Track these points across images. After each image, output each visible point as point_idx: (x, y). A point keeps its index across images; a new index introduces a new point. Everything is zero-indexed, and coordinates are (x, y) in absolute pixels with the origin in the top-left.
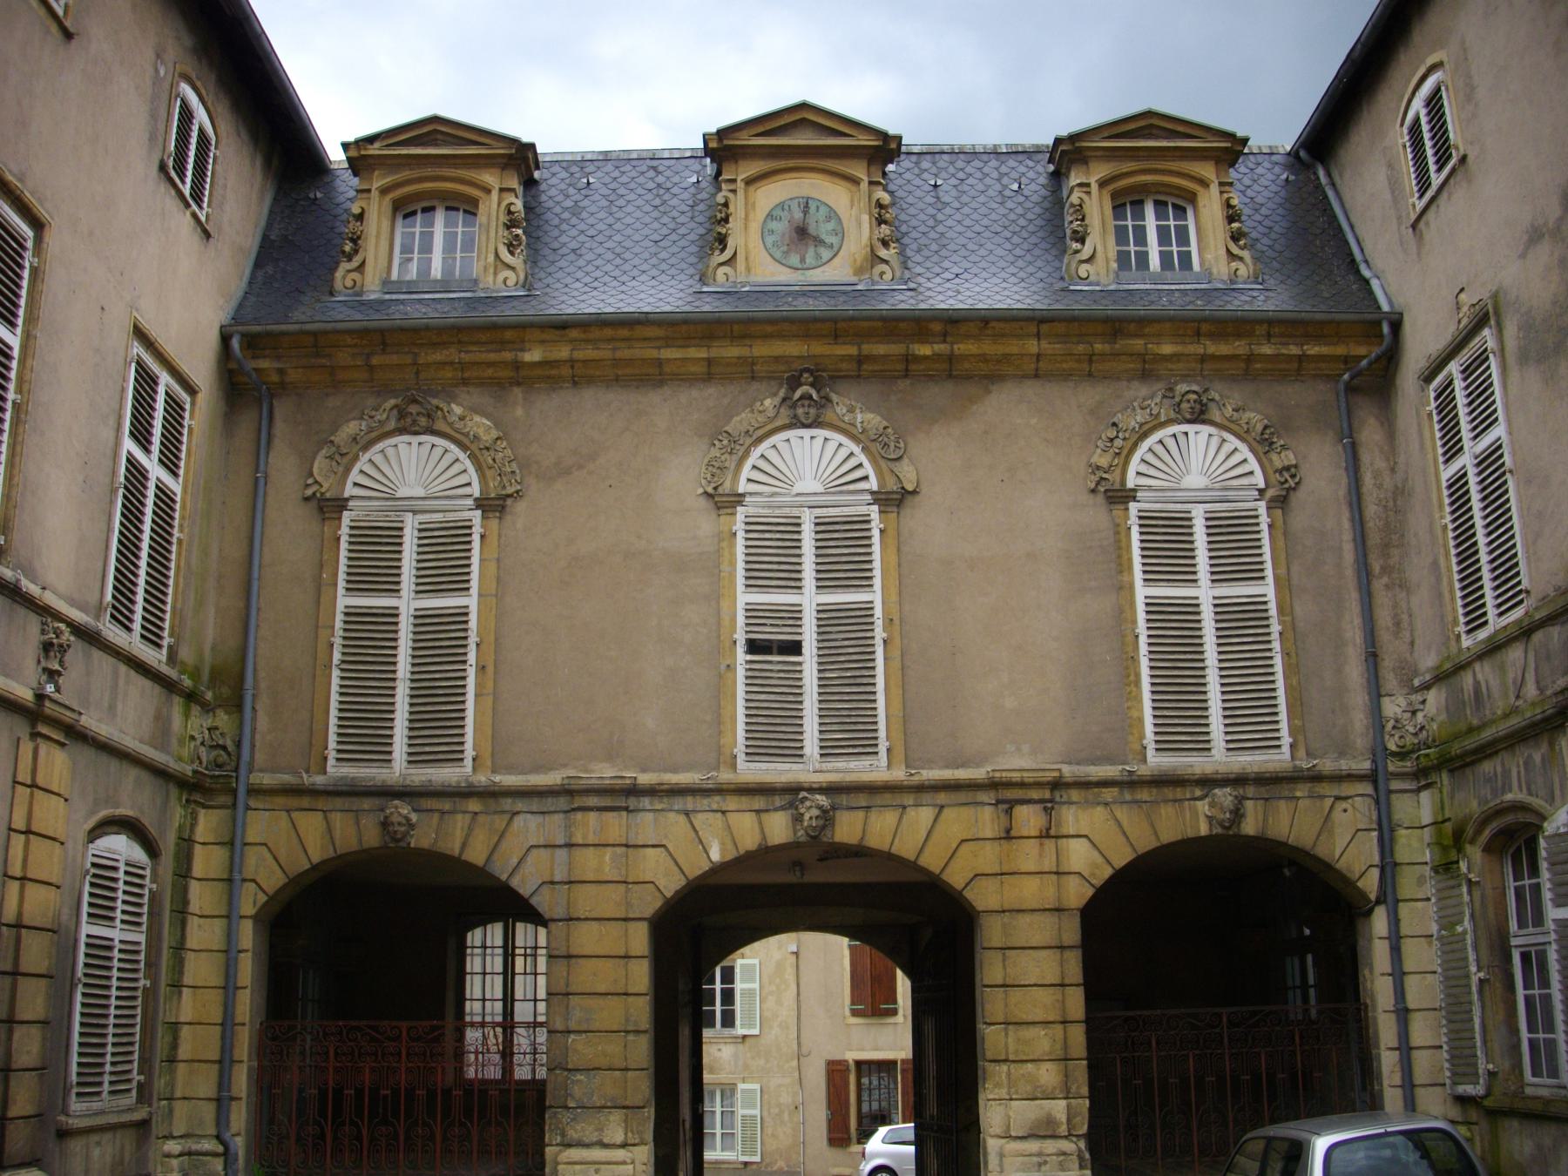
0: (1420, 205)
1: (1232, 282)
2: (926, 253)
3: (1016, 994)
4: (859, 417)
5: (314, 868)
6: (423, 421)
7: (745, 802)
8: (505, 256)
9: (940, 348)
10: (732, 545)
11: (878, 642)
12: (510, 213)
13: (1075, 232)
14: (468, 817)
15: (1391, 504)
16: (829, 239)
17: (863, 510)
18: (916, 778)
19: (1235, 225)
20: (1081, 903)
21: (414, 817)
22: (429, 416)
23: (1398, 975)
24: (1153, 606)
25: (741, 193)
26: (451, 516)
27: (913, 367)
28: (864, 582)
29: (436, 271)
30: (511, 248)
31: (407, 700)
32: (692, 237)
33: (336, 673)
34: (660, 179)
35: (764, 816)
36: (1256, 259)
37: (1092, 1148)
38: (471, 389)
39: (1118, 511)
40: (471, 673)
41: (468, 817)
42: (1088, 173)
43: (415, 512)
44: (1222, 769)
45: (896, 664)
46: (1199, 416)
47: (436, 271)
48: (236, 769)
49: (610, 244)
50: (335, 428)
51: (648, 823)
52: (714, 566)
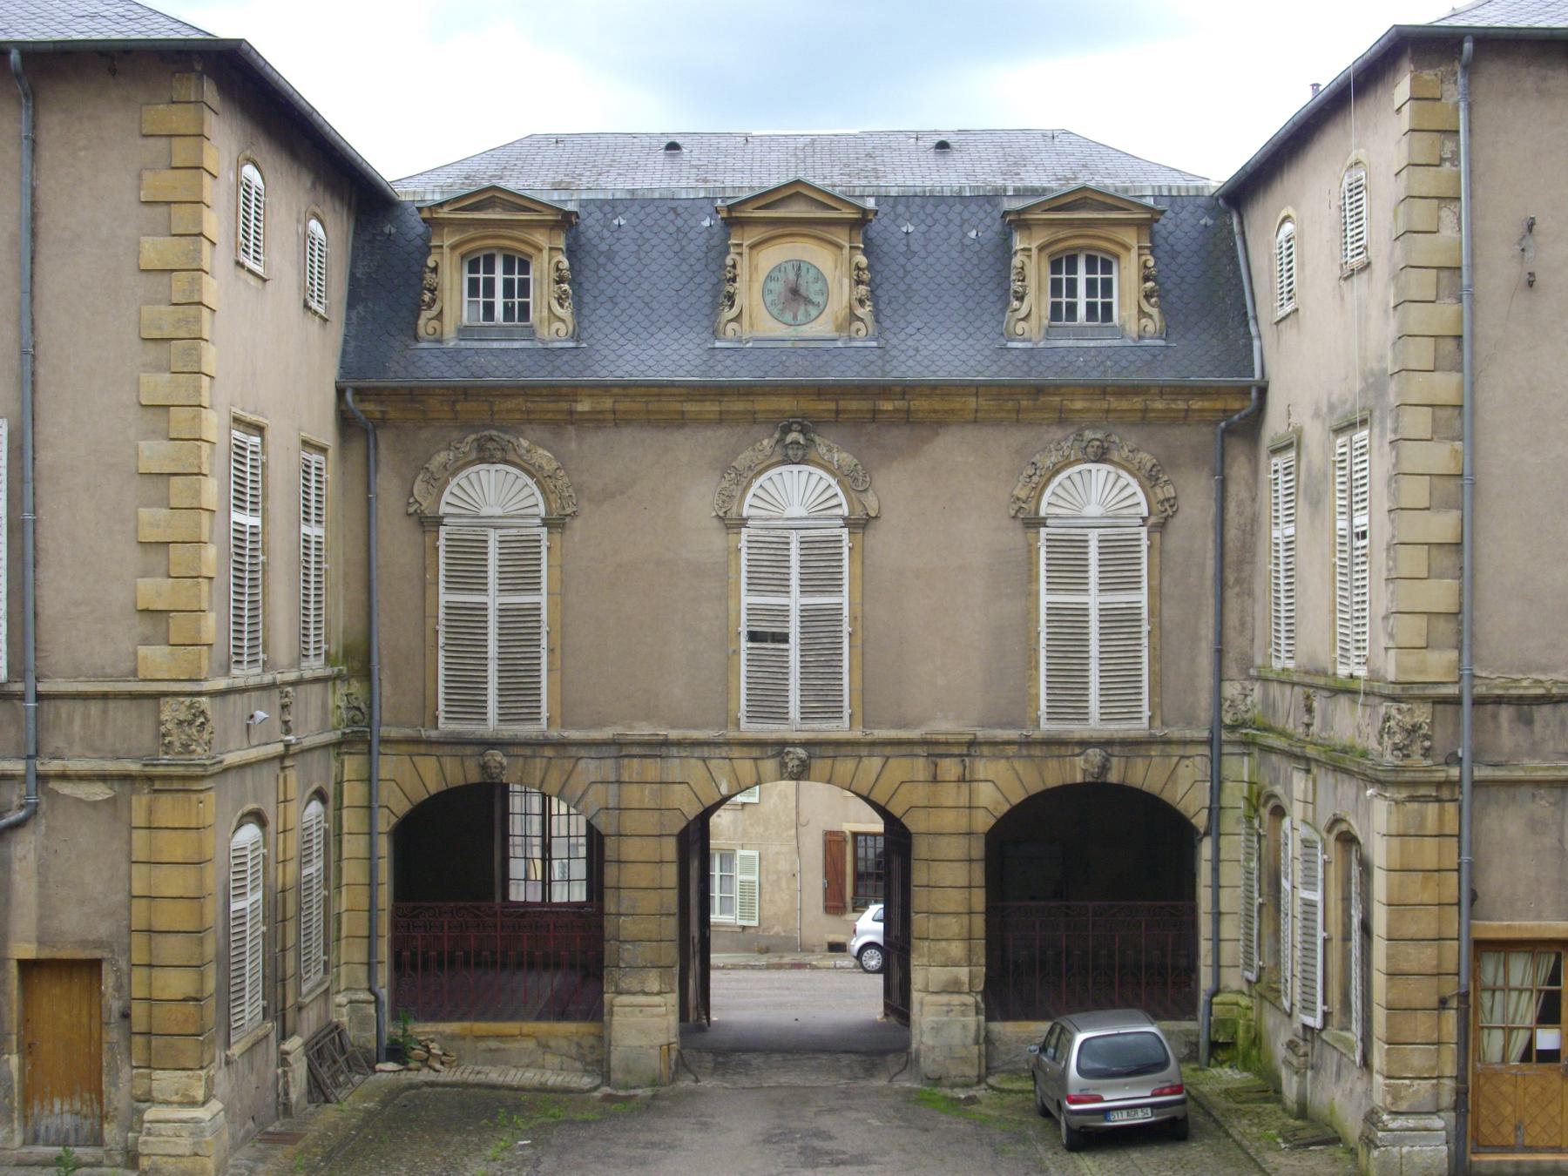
1: (1140, 337)
2: (895, 305)
3: (936, 893)
6: (499, 454)
7: (745, 751)
9: (900, 404)
10: (738, 558)
11: (845, 635)
12: (558, 269)
16: (816, 299)
17: (837, 531)
20: (987, 828)
23: (1216, 887)
24: (1053, 610)
25: (746, 257)
26: (524, 531)
33: (441, 653)
34: (679, 222)
35: (760, 763)
36: (1163, 312)
39: (1031, 534)
43: (496, 528)
44: (1095, 735)
45: (858, 651)
46: (1102, 457)
48: (369, 726)
51: (674, 768)
52: (724, 573)
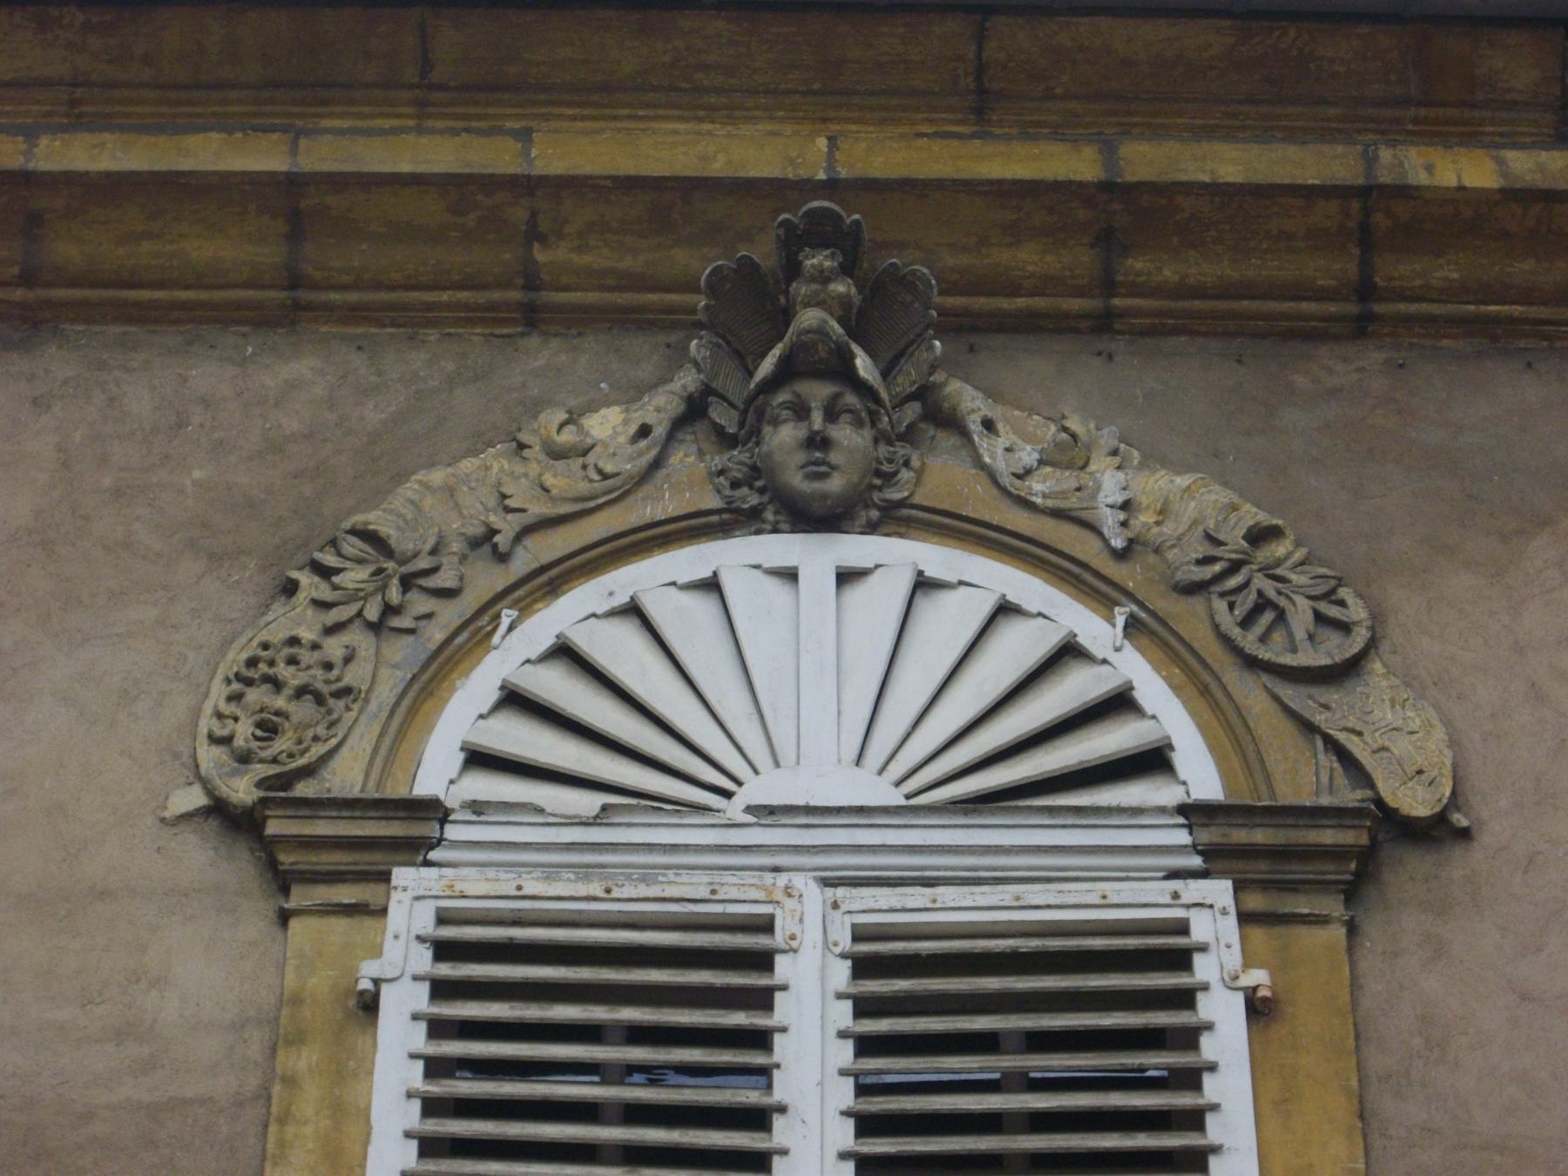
4: (1110, 485)
17: (1142, 899)
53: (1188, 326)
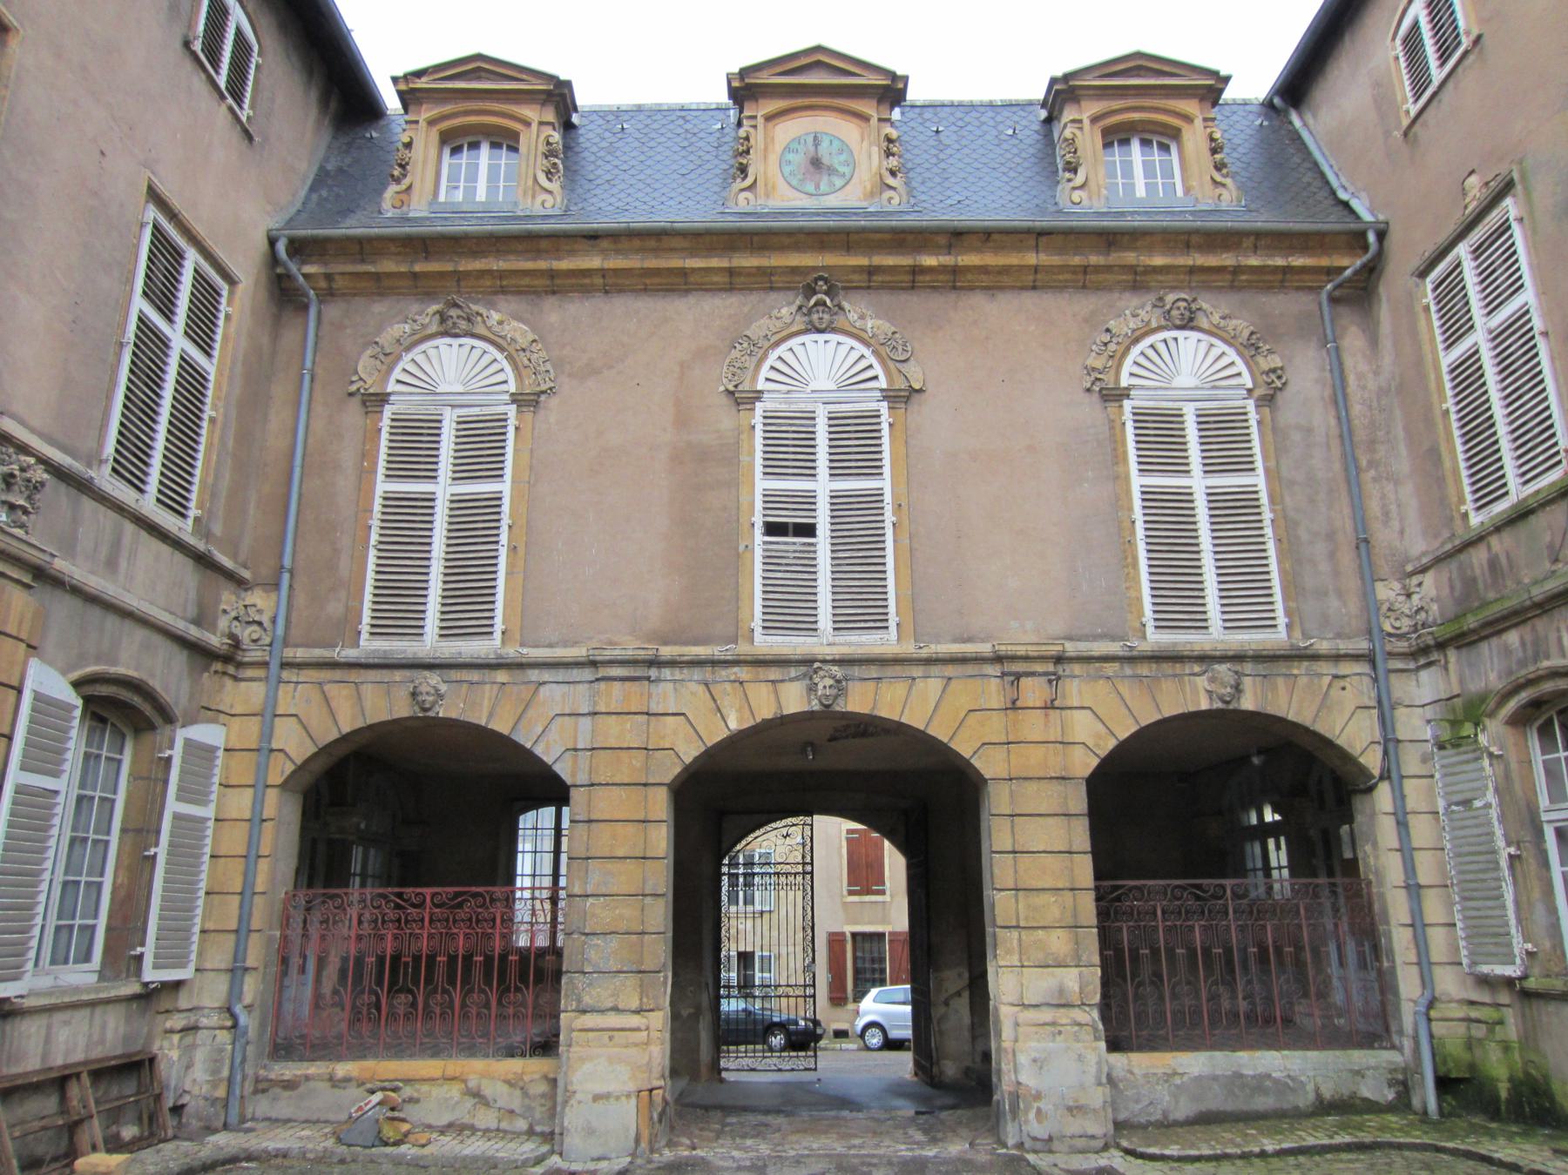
0: (1413, 111)
5: (344, 738)
6: (463, 325)
8: (546, 184)
12: (548, 143)
13: (1069, 163)
14: (496, 687)
15: (1375, 404)
16: (842, 169)
17: (874, 406)
18: (925, 651)
19: (1218, 156)
20: (1087, 772)
21: (443, 688)
22: (469, 320)
23: (1407, 852)
24: (1148, 495)
26: (486, 410)
27: (920, 278)
28: (874, 470)
29: (481, 195)
30: (549, 175)
31: (441, 577)
32: (718, 171)
33: (372, 553)
34: (688, 126)
35: (779, 686)
37: (1105, 1018)
38: (510, 297)
39: (1112, 407)
40: (503, 553)
41: (496, 687)
42: (1081, 112)
46: (1188, 324)
47: (481, 195)
49: (642, 177)
50: (380, 329)
52: (730, 455)
53: (883, 288)
